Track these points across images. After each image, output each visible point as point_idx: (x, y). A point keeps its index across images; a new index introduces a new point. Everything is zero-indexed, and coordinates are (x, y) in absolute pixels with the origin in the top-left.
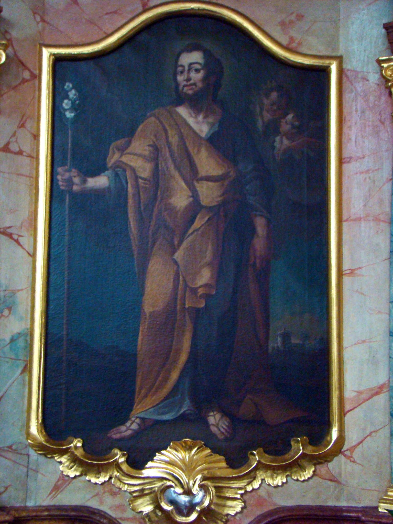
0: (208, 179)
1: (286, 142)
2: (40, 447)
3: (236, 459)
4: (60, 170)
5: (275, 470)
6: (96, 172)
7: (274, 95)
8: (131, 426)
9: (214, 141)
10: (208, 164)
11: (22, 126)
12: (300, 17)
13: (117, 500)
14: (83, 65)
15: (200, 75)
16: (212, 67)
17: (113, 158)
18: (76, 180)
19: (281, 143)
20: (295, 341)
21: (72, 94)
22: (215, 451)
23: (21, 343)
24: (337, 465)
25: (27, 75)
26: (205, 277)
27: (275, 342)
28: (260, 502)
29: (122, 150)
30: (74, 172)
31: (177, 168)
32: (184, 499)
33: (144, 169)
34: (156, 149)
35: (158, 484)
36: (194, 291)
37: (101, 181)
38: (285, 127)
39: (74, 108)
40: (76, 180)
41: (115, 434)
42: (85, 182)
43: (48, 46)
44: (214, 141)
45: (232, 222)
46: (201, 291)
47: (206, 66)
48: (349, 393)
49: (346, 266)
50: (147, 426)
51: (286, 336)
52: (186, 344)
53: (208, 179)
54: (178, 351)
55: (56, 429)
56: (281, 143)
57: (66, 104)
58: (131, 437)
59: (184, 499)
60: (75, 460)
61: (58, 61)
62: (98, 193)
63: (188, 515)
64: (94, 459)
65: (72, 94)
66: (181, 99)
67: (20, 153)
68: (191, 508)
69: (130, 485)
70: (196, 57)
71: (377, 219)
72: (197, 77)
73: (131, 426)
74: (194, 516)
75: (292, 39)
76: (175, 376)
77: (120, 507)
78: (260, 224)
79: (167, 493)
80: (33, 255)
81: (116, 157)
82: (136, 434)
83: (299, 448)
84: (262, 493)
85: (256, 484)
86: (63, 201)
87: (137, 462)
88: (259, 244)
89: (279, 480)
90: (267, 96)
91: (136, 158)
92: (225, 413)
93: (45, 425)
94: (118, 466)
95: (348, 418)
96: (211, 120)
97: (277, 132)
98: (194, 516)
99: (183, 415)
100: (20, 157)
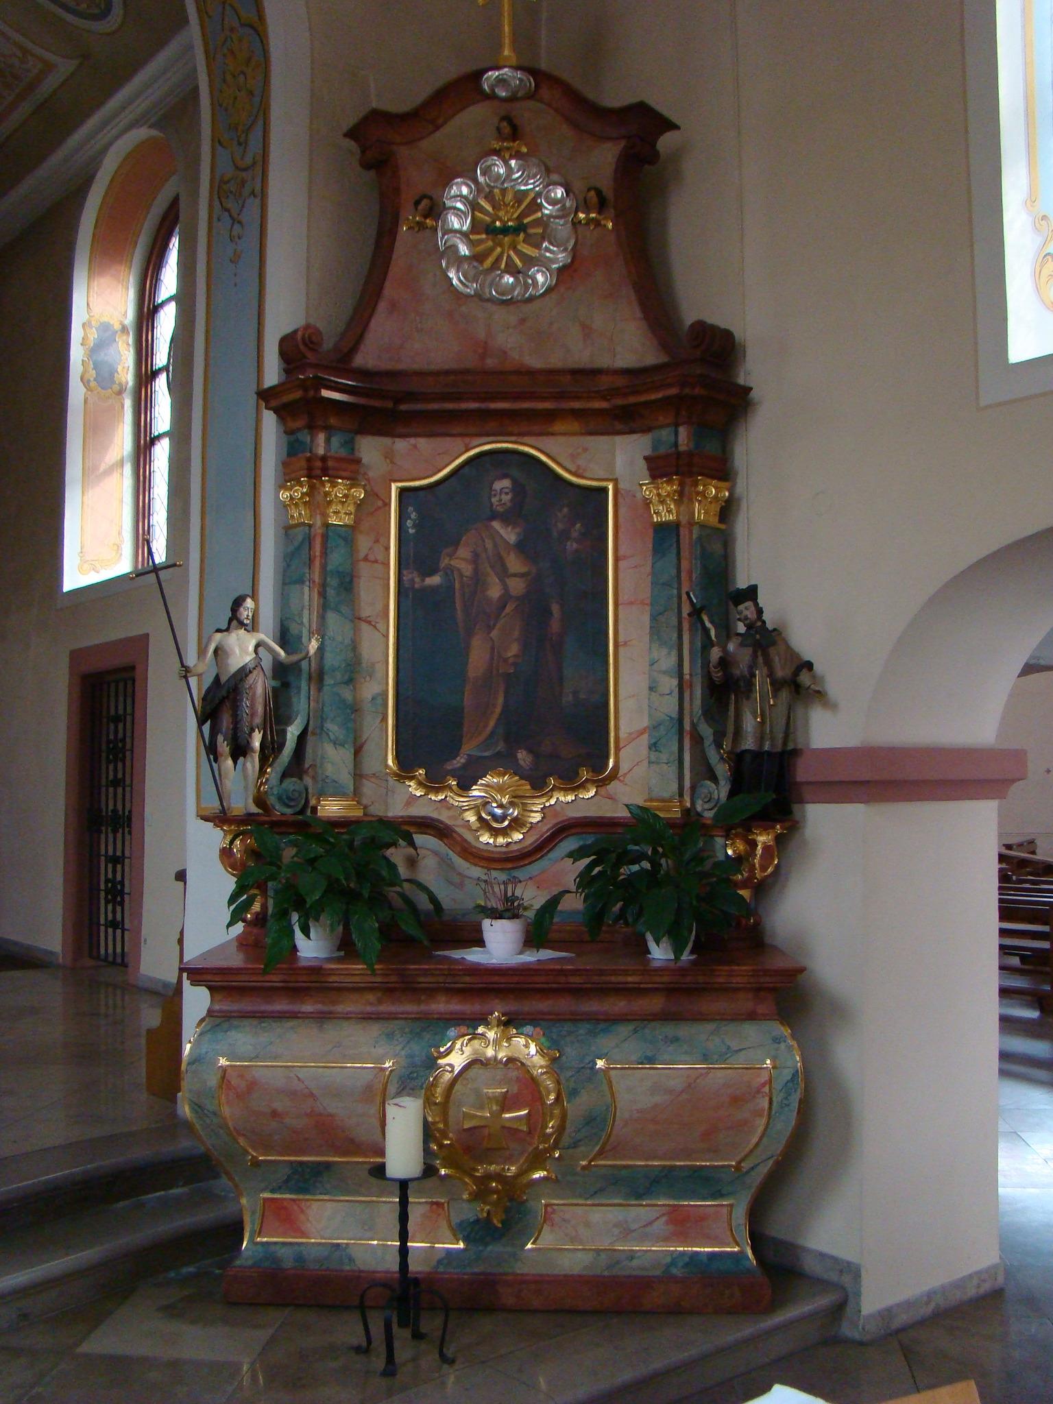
0: (515, 575)
1: (575, 545)
2: (396, 775)
3: (538, 785)
4: (405, 572)
5: (566, 790)
6: (432, 573)
7: (565, 510)
8: (460, 760)
9: (520, 547)
10: (515, 564)
11: (377, 541)
12: (585, 450)
13: (451, 813)
14: (421, 493)
15: (509, 497)
16: (518, 490)
17: (445, 562)
18: (417, 580)
19: (571, 546)
20: (582, 696)
21: (413, 516)
22: (521, 778)
23: (379, 701)
24: (613, 786)
25: (380, 503)
26: (514, 649)
27: (568, 698)
28: (556, 814)
29: (451, 556)
30: (415, 574)
31: (492, 567)
32: (499, 811)
33: (467, 570)
34: (476, 556)
35: (480, 801)
36: (505, 660)
37: (435, 580)
38: (575, 534)
39: (414, 526)
40: (417, 580)
41: (449, 767)
42: (423, 581)
43: (395, 481)
44: (520, 547)
45: (534, 609)
46: (511, 661)
47: (513, 490)
48: (623, 734)
49: (621, 639)
50: (471, 760)
51: (575, 693)
52: (501, 700)
53: (515, 575)
54: (494, 706)
55: (406, 765)
56: (571, 546)
57: (409, 523)
58: (459, 769)
59: (499, 811)
60: (420, 784)
61: (402, 492)
62: (434, 589)
63: (503, 821)
64: (434, 783)
65: (413, 516)
66: (494, 516)
67: (376, 561)
68: (504, 818)
69: (458, 801)
70: (506, 483)
71: (642, 603)
72: (506, 498)
73: (460, 760)
74: (506, 823)
75: (579, 467)
76: (492, 723)
77: (454, 818)
78: (555, 609)
79: (488, 807)
80: (387, 637)
81: (446, 561)
82: (465, 766)
83: (585, 774)
84: (558, 808)
85: (553, 802)
86: (407, 596)
87: (465, 787)
88: (555, 626)
89: (570, 798)
90: (560, 511)
91: (460, 561)
92: (530, 750)
93: (398, 757)
94: (450, 787)
95: (622, 753)
96: (518, 530)
97: (568, 538)
98: (506, 823)
99: (499, 753)
100: (376, 565)
